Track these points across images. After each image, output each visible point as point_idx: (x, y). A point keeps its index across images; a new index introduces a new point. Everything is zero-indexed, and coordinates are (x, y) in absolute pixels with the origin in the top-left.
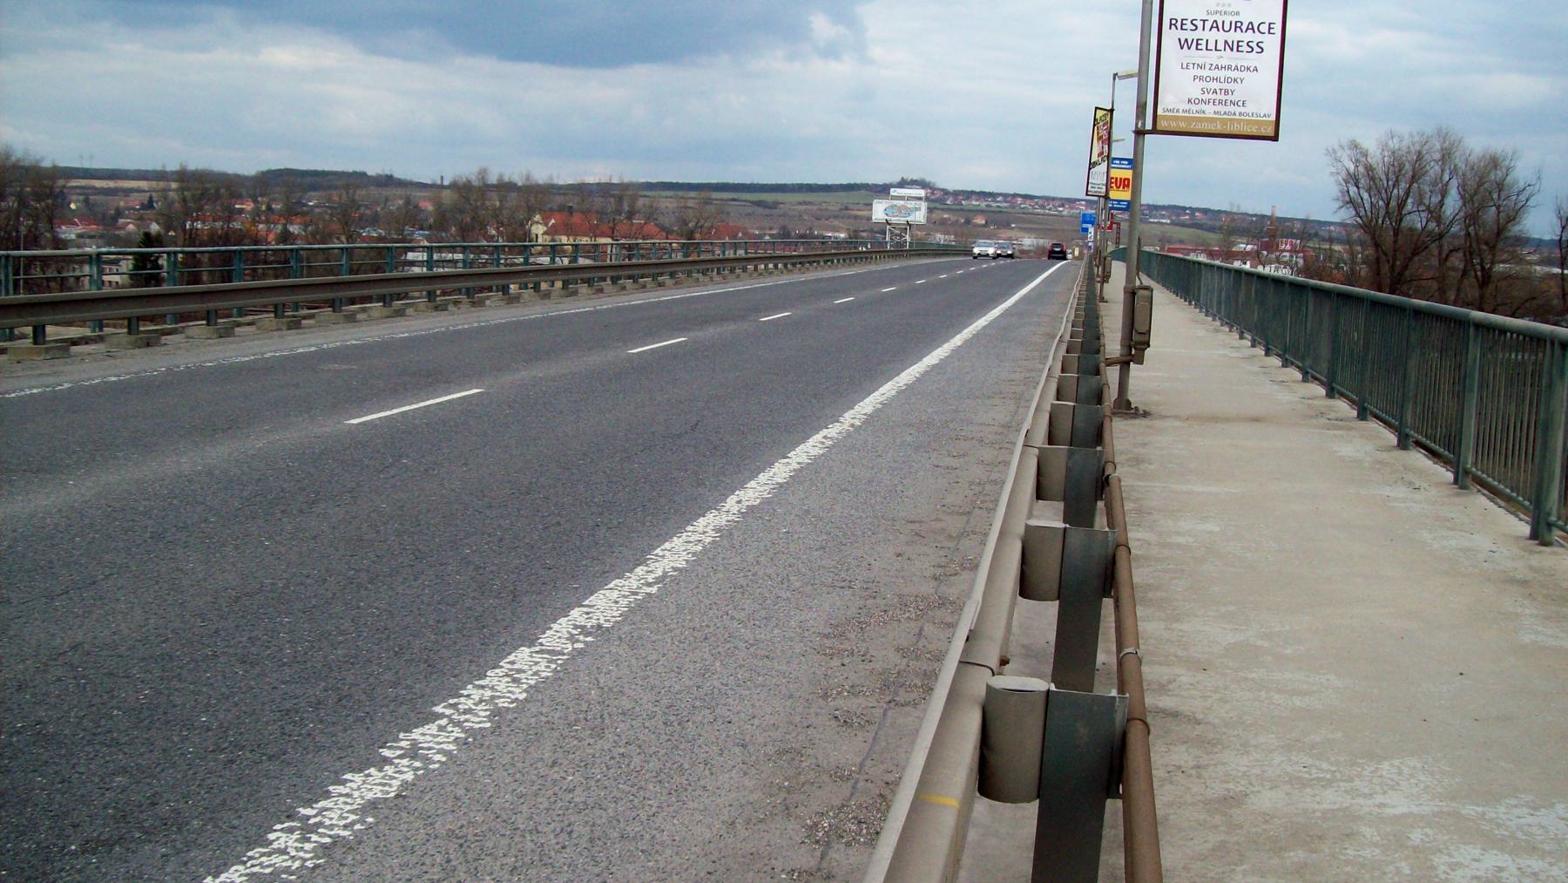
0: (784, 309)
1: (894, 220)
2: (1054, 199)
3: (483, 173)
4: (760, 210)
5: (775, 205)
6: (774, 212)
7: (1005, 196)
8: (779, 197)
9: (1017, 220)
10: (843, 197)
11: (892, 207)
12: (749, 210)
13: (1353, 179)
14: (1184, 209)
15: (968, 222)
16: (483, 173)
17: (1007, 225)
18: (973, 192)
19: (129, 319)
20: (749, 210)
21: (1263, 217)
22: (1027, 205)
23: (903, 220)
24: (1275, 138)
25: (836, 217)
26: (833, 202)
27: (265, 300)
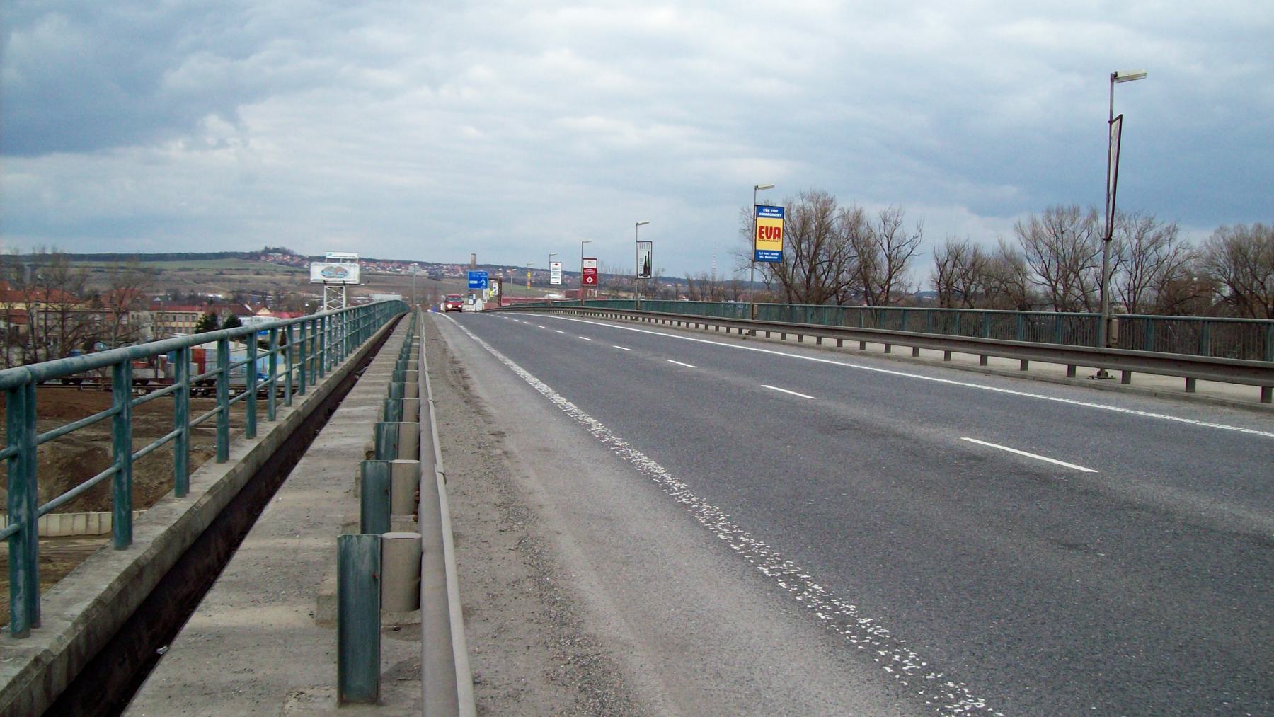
0: (769, 396)
1: (331, 280)
2: (392, 262)
5: (160, 271)
8: (158, 265)
11: (329, 268)
13: (825, 194)
14: (498, 267)
21: (622, 276)
23: (338, 280)
24: (1114, 77)
25: (213, 280)
26: (209, 268)
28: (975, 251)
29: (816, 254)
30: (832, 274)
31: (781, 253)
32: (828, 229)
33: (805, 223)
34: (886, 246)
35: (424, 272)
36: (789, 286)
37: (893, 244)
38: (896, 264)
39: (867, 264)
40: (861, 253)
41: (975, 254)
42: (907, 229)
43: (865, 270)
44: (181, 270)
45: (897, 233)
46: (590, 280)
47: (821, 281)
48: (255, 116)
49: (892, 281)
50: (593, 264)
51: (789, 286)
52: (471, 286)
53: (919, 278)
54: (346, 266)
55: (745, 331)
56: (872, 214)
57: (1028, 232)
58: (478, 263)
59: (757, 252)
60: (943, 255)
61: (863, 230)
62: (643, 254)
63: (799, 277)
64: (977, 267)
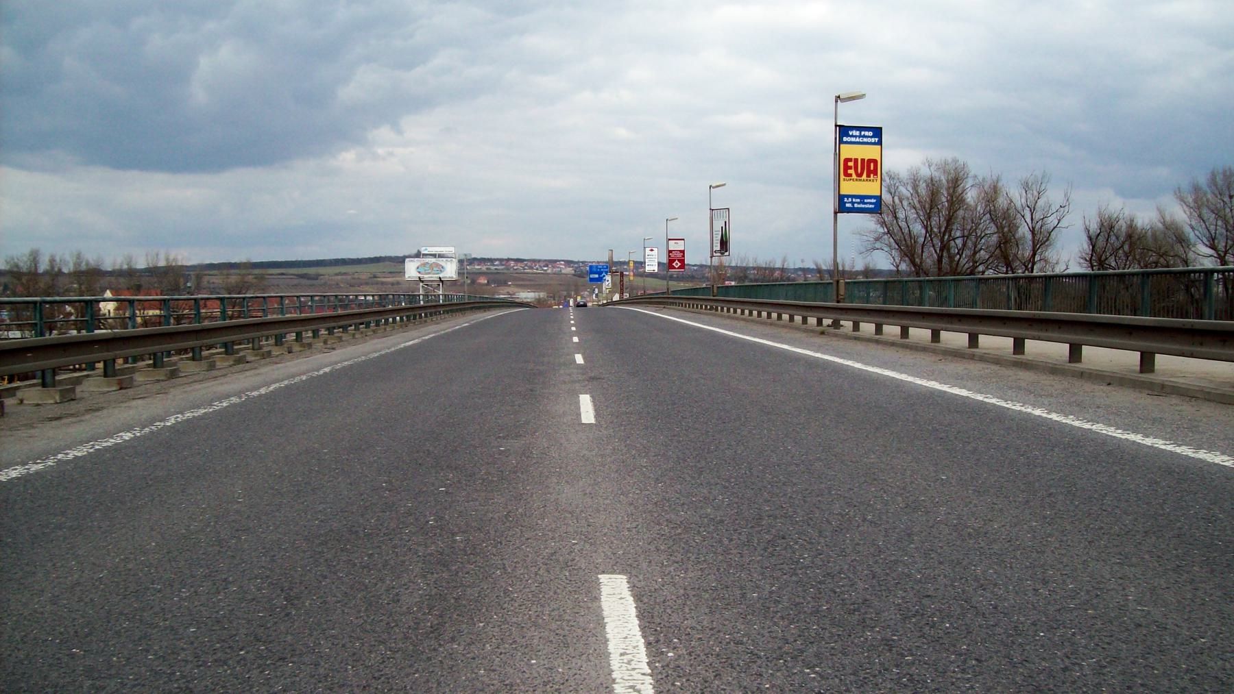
1: (426, 277)
2: (539, 261)
3: (34, 257)
4: (304, 281)
5: (317, 277)
6: (315, 282)
7: (501, 260)
8: (321, 270)
9: (515, 279)
10: (373, 268)
11: (424, 264)
12: (296, 281)
15: (473, 282)
16: (34, 257)
17: (505, 284)
18: (475, 259)
19: (155, 354)
20: (296, 281)
21: (702, 266)
22: (519, 266)
23: (435, 277)
25: (367, 284)
26: (364, 272)
27: (241, 336)
28: (1132, 221)
29: (948, 229)
30: (967, 253)
31: (879, 198)
32: (961, 201)
33: (934, 194)
34: (1029, 220)
35: (569, 270)
36: (918, 269)
37: (1037, 216)
38: (1041, 239)
39: (1007, 241)
40: (1000, 228)
41: (1131, 226)
42: (1053, 196)
43: (1005, 249)
44: (337, 274)
45: (1041, 203)
46: (677, 264)
47: (956, 264)
48: (418, 127)
49: (1037, 258)
50: (679, 246)
51: (918, 269)
52: (592, 280)
53: (1068, 256)
54: (441, 261)
55: (827, 322)
56: (1014, 194)
57: (1190, 200)
58: (615, 259)
59: (841, 198)
60: (1094, 227)
61: (1002, 202)
62: (718, 225)
63: (929, 257)
64: (1134, 239)
